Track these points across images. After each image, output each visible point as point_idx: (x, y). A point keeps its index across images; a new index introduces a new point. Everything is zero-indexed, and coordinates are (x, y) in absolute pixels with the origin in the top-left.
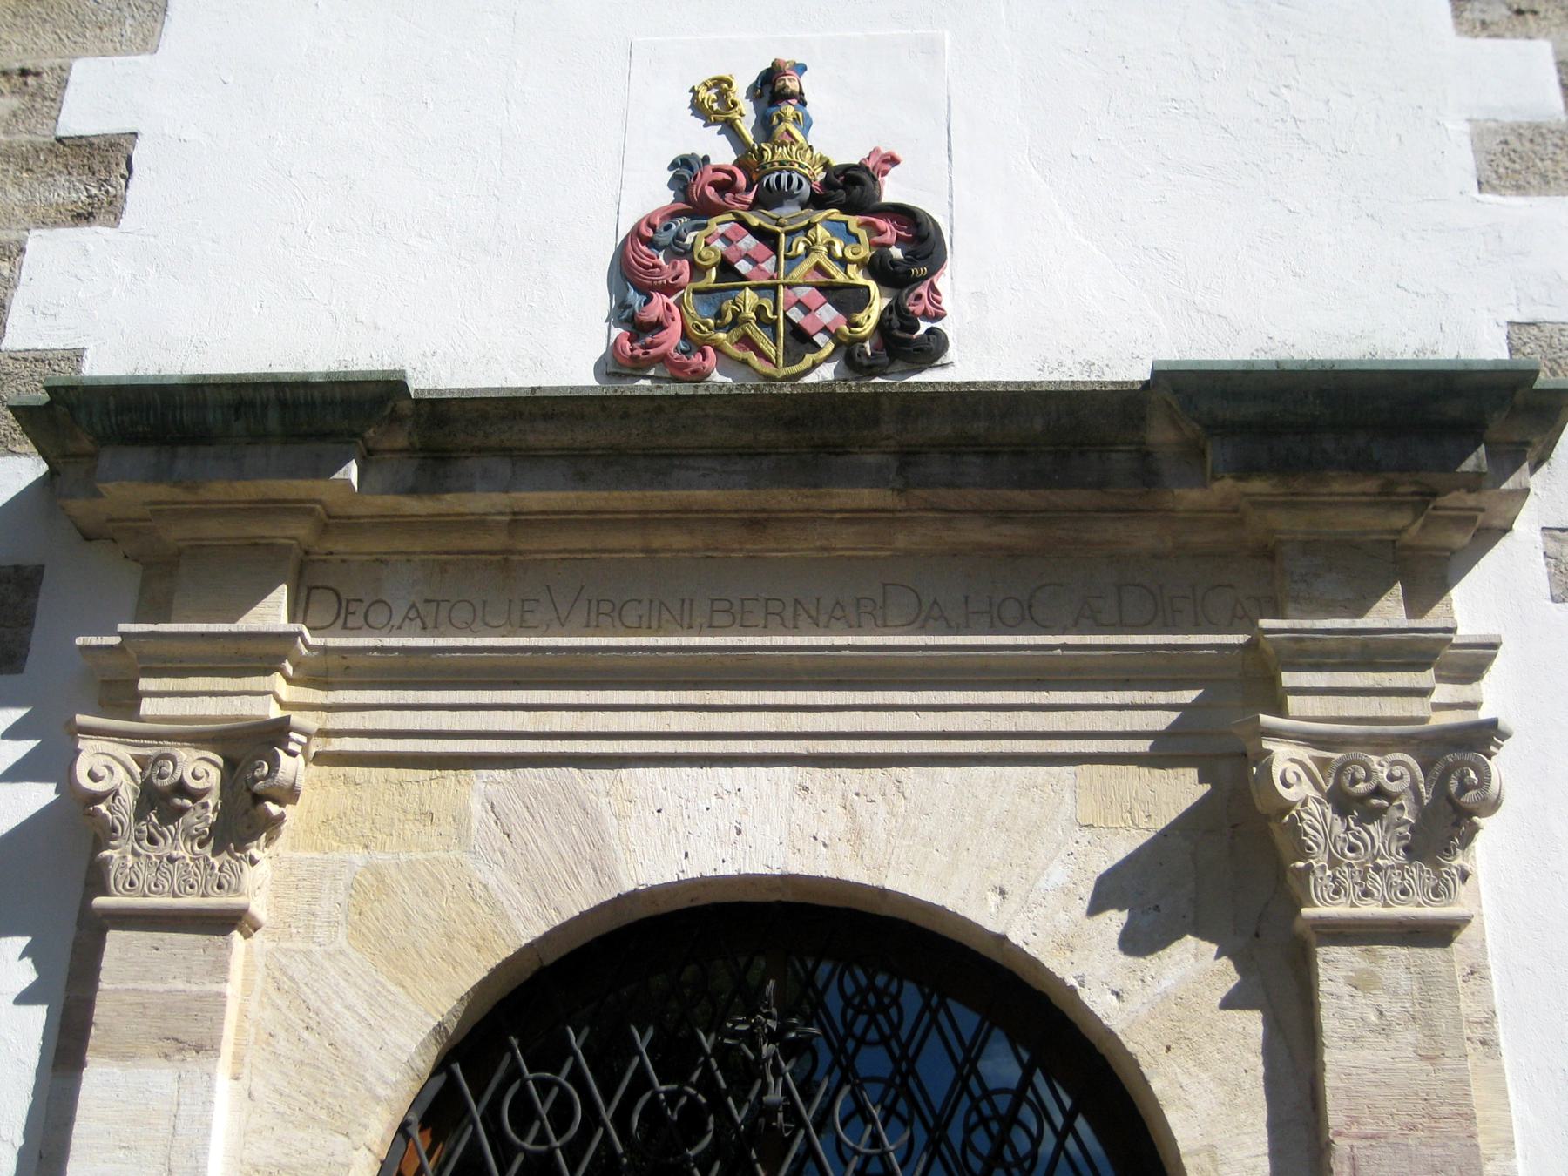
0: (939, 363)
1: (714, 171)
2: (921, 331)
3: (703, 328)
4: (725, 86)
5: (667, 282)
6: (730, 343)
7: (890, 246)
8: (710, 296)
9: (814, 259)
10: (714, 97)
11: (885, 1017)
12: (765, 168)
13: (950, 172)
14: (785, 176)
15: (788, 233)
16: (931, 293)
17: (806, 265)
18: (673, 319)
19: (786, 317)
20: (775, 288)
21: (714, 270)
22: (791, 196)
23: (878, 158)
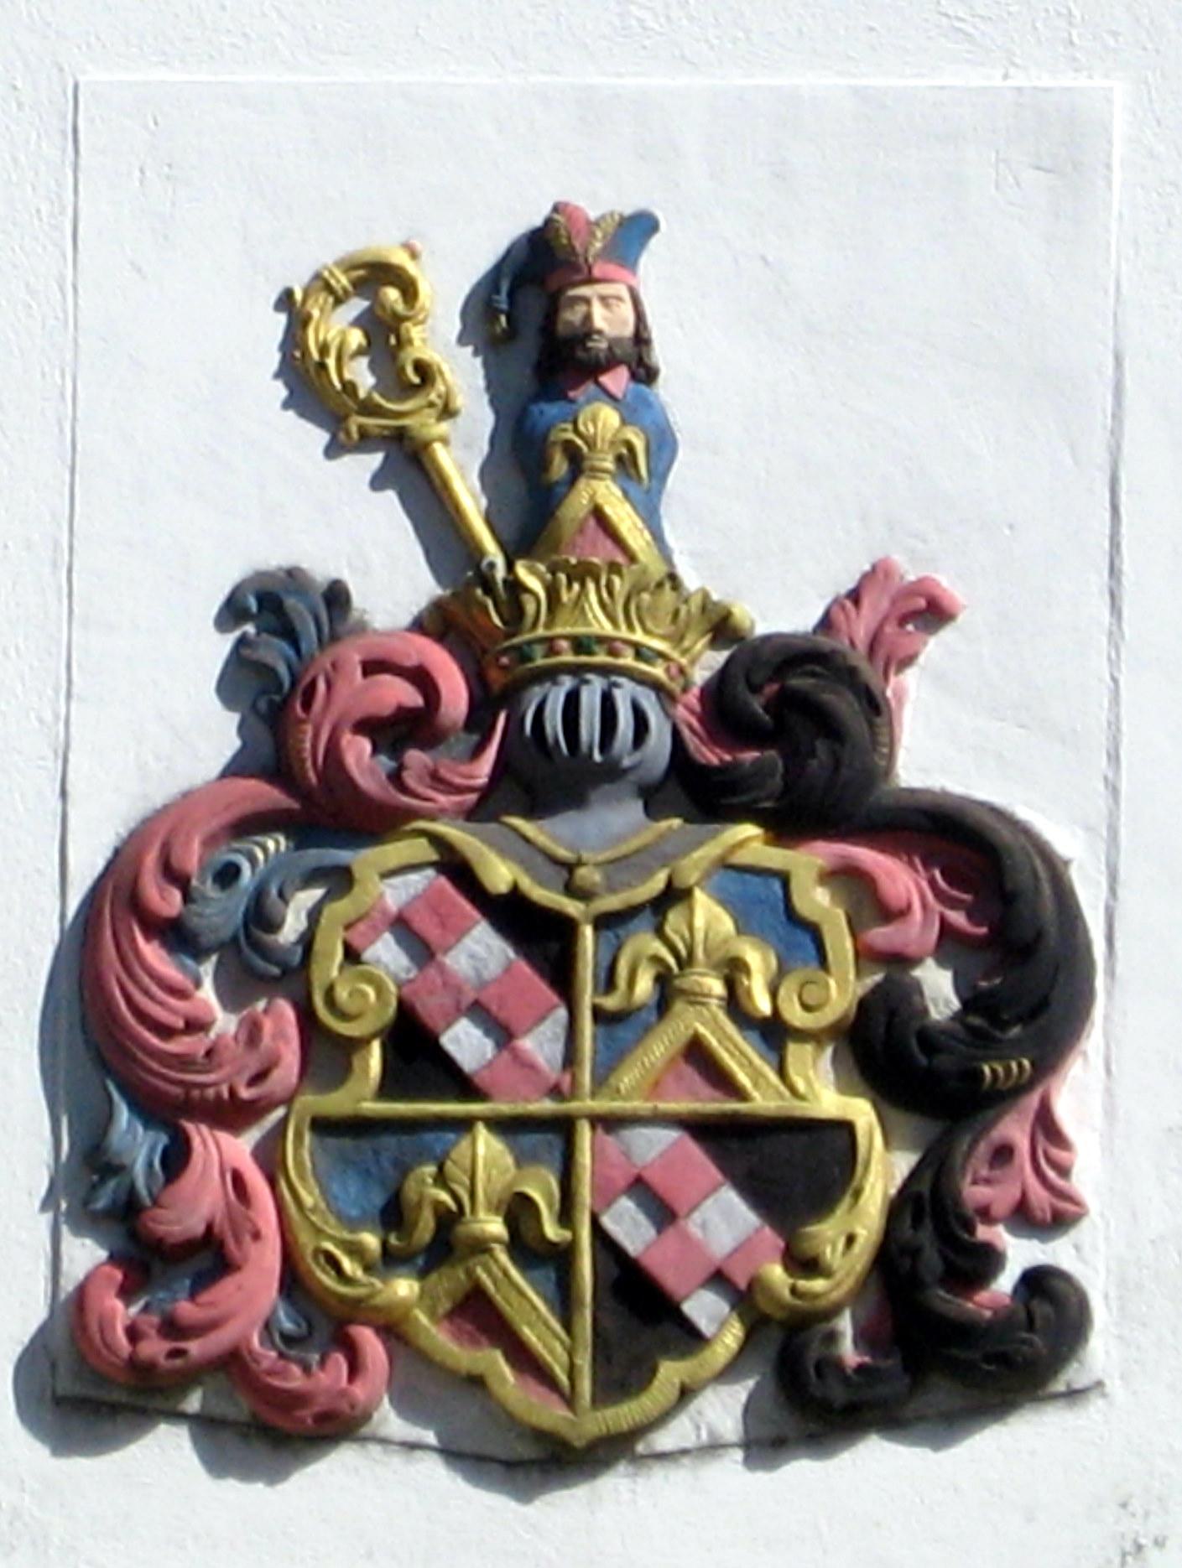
0: (1059, 1386)
1: (371, 667)
2: (1005, 1283)
3: (347, 1265)
4: (392, 294)
5: (232, 1092)
6: (432, 1314)
7: (914, 961)
8: (366, 1144)
9: (686, 1022)
10: (356, 338)
11: (296, 1006)
12: (528, 658)
13: (1114, 663)
14: (590, 700)
15: (603, 922)
16: (1042, 1143)
17: (661, 1046)
18: (257, 1236)
19: (598, 1230)
20: (563, 1127)
21: (376, 1047)
22: (612, 772)
23: (885, 604)
